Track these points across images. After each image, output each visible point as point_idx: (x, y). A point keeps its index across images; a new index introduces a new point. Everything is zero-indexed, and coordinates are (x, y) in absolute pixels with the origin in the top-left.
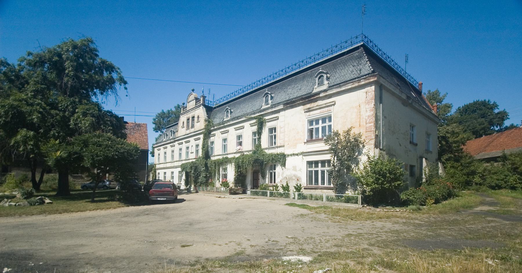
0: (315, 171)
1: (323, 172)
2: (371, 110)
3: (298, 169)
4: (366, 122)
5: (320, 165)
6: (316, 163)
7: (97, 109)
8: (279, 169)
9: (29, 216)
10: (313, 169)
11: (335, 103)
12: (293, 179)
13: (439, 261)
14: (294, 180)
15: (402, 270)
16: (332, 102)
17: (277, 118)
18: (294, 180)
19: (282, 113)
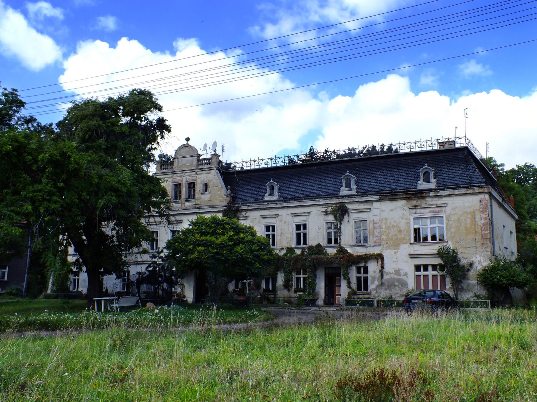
0: (424, 276)
1: (434, 276)
2: (486, 219)
3: (402, 273)
4: (482, 229)
5: (430, 268)
6: (426, 268)
7: (217, 282)
8: (194, 221)
9: (380, 19)
10: (422, 273)
11: (447, 205)
12: (395, 286)
13: (197, 240)
14: (397, 286)
15: (532, 385)
16: (445, 204)
17: (368, 210)
18: (397, 286)
19: (376, 205)
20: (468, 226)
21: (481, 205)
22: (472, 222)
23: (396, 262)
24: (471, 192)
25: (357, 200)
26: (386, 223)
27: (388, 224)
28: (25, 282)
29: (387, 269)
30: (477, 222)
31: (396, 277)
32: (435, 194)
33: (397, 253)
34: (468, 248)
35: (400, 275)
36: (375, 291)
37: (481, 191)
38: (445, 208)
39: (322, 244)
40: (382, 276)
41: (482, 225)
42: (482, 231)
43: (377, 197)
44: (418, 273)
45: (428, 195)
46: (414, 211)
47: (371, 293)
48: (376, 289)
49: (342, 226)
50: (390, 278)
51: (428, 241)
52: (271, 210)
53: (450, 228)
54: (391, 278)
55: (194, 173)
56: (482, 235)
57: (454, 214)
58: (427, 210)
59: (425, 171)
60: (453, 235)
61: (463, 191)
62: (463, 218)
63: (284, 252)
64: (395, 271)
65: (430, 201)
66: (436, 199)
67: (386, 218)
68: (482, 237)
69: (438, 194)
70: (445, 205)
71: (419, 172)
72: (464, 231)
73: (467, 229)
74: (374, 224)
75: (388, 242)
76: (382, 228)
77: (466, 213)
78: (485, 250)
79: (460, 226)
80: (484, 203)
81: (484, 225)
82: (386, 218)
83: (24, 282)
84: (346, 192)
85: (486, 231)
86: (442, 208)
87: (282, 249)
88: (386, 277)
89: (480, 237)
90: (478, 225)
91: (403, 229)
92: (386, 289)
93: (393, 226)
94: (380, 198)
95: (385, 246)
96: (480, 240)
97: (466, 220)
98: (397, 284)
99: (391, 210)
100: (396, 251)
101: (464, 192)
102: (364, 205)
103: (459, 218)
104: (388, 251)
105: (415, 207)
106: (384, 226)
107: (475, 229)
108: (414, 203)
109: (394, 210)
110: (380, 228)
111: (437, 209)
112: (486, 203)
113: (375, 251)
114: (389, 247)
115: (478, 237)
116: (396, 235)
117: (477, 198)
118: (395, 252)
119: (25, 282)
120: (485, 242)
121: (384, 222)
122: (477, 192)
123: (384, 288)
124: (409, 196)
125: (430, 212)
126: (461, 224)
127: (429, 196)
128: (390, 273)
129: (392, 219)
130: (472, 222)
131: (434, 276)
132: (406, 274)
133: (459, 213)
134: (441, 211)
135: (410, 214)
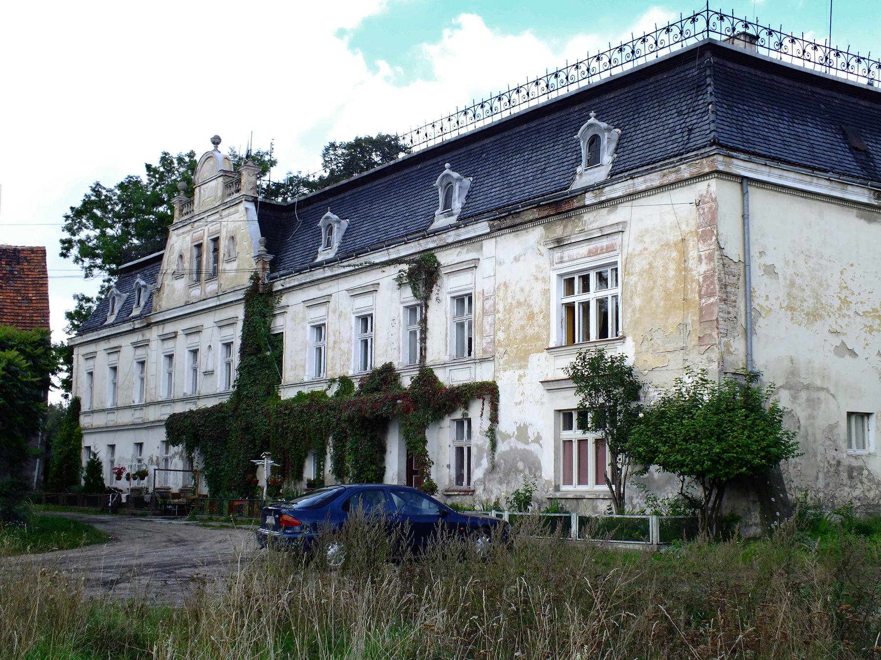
2: (710, 258)
3: (531, 434)
4: (700, 291)
19: (489, 245)
20: (671, 284)
21: (700, 215)
22: (681, 272)
23: (520, 403)
24: (672, 177)
25: (450, 240)
26: (505, 298)
27: (510, 300)
28: (37, 470)
29: (506, 424)
30: (691, 270)
31: (521, 446)
32: (595, 197)
33: (523, 380)
34: (669, 356)
35: (527, 443)
36: (482, 487)
37: (695, 171)
38: (619, 236)
39: (396, 365)
40: (494, 446)
41: (701, 280)
42: (701, 297)
43: (483, 227)
44: (567, 435)
45: (580, 204)
46: (557, 254)
47: (474, 491)
48: (483, 481)
49: (429, 315)
50: (508, 448)
51: (591, 340)
52: (322, 286)
53: (631, 297)
54: (511, 448)
55: (217, 216)
56: (701, 309)
57: (641, 254)
58: (584, 249)
59: (590, 133)
60: (638, 315)
61: (655, 179)
62: (659, 263)
63: (335, 388)
64: (519, 429)
65: (594, 220)
66: (604, 212)
67: (505, 284)
68: (701, 316)
69: (603, 198)
70: (620, 230)
71: (578, 142)
72: (662, 304)
73: (668, 296)
74: (483, 301)
75: (509, 349)
76: (498, 312)
77: (667, 245)
78: (705, 356)
79: (652, 289)
80: (706, 207)
81: (705, 278)
82: (505, 284)
83: (35, 470)
84: (444, 220)
85: (711, 295)
86: (615, 237)
87: (333, 381)
88: (502, 447)
89: (696, 318)
90: (693, 281)
91: (536, 310)
92: (501, 482)
93: (519, 304)
94: (491, 226)
95: (502, 361)
96: (697, 326)
97: (666, 269)
98: (520, 465)
99: (516, 259)
100: (521, 372)
101: (657, 183)
102: (468, 251)
103: (650, 264)
104: (509, 373)
105: (559, 243)
106: (500, 307)
107: (685, 294)
108: (559, 231)
109: (522, 258)
110: (496, 311)
111: (605, 242)
112: (710, 208)
113: (482, 374)
114: (508, 365)
115: (692, 318)
116: (523, 328)
117: (685, 196)
118: (520, 376)
119: (37, 470)
120: (708, 332)
121: (501, 293)
122: (687, 175)
123: (496, 476)
124: (545, 213)
125: (591, 254)
126: (654, 282)
127: (585, 206)
128: (510, 437)
129: (516, 284)
130: (681, 272)
131: (582, 443)
132: (538, 439)
133: (653, 248)
134: (610, 249)
135: (552, 264)
